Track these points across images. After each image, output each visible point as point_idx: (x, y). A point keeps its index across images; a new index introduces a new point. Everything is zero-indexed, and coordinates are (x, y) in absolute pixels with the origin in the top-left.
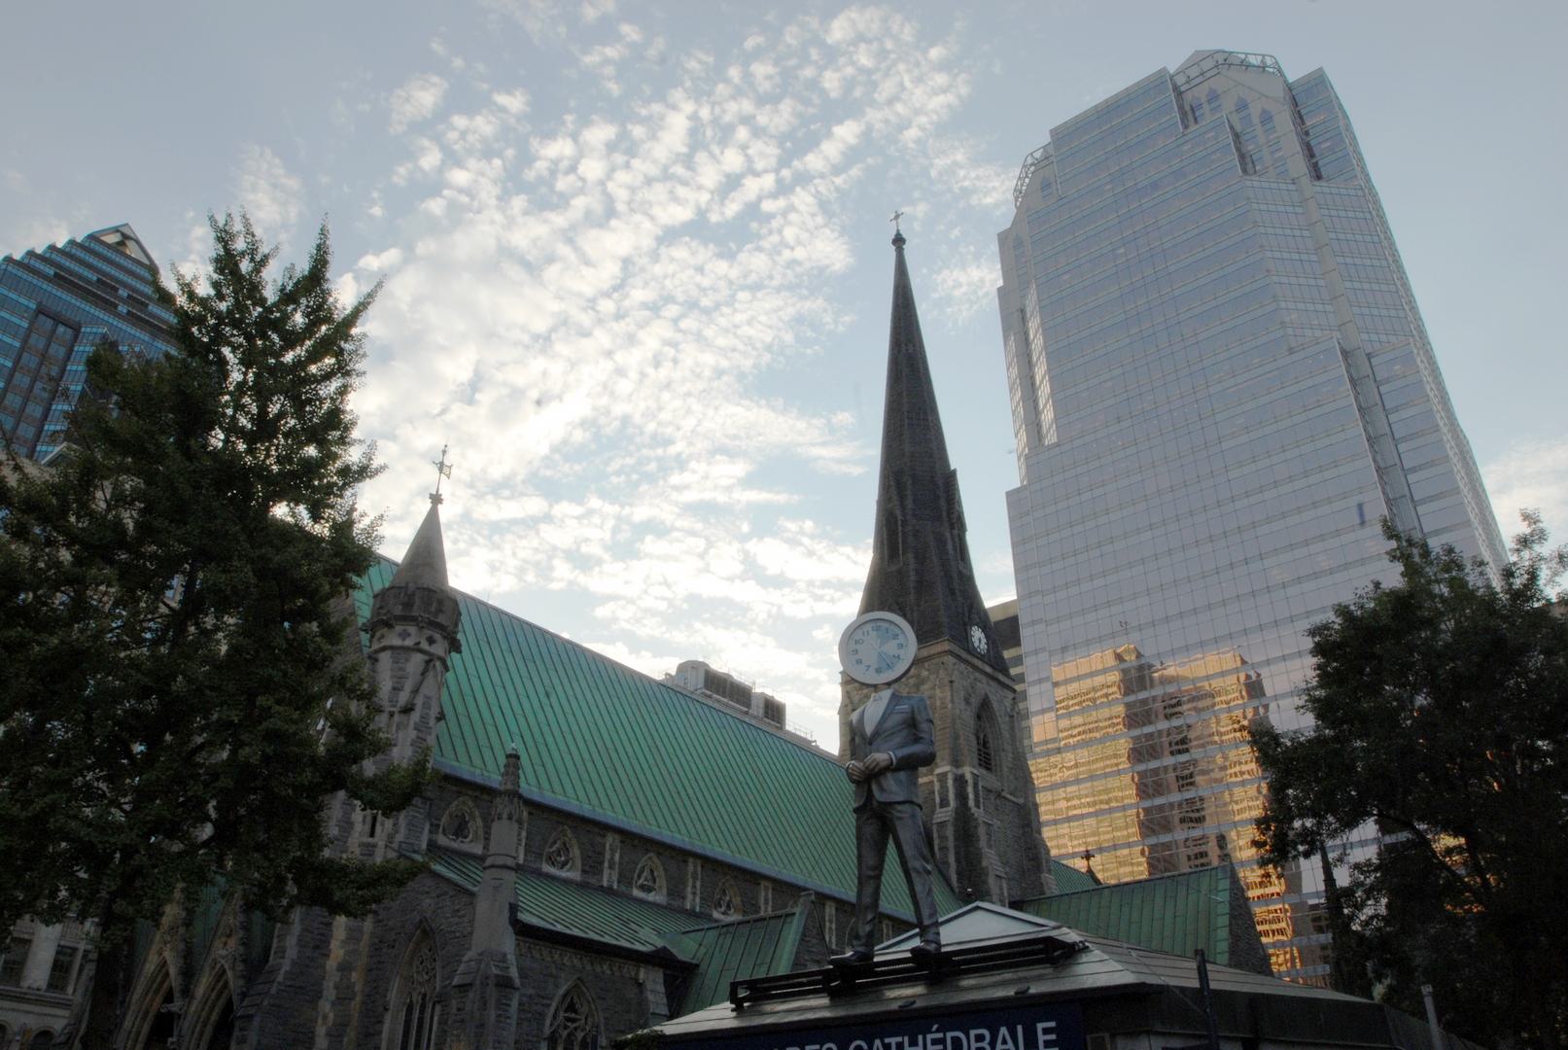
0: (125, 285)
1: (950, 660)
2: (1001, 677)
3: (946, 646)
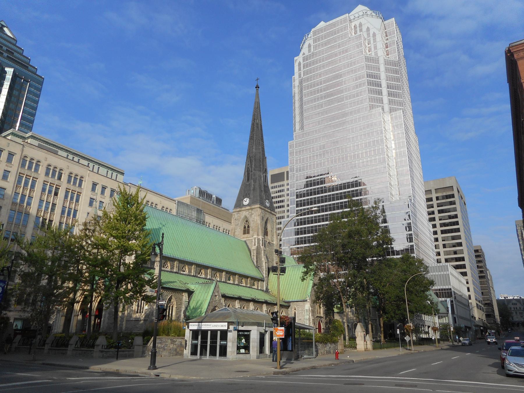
0: (6, 46)
1: (258, 209)
2: (273, 212)
3: (258, 206)
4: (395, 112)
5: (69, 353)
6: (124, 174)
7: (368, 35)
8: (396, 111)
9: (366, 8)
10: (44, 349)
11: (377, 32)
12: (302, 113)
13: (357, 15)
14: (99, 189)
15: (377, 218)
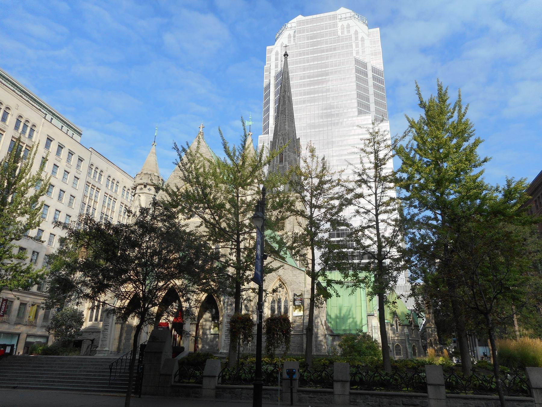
6: (81, 134)
7: (357, 38)
11: (365, 37)
13: (344, 16)
14: (54, 146)
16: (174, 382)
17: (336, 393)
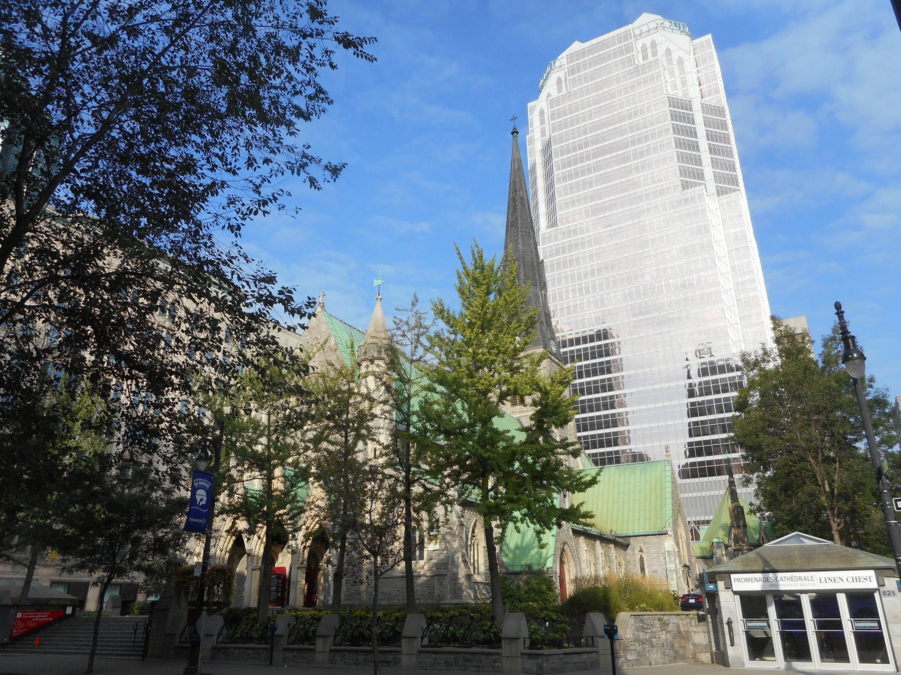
4: (727, 196)
5: (319, 657)
7: (670, 61)
8: (727, 193)
9: (659, 17)
10: (313, 650)
11: (685, 56)
12: (551, 200)
13: (645, 29)
15: (364, 438)
16: (180, 642)
17: (317, 650)
